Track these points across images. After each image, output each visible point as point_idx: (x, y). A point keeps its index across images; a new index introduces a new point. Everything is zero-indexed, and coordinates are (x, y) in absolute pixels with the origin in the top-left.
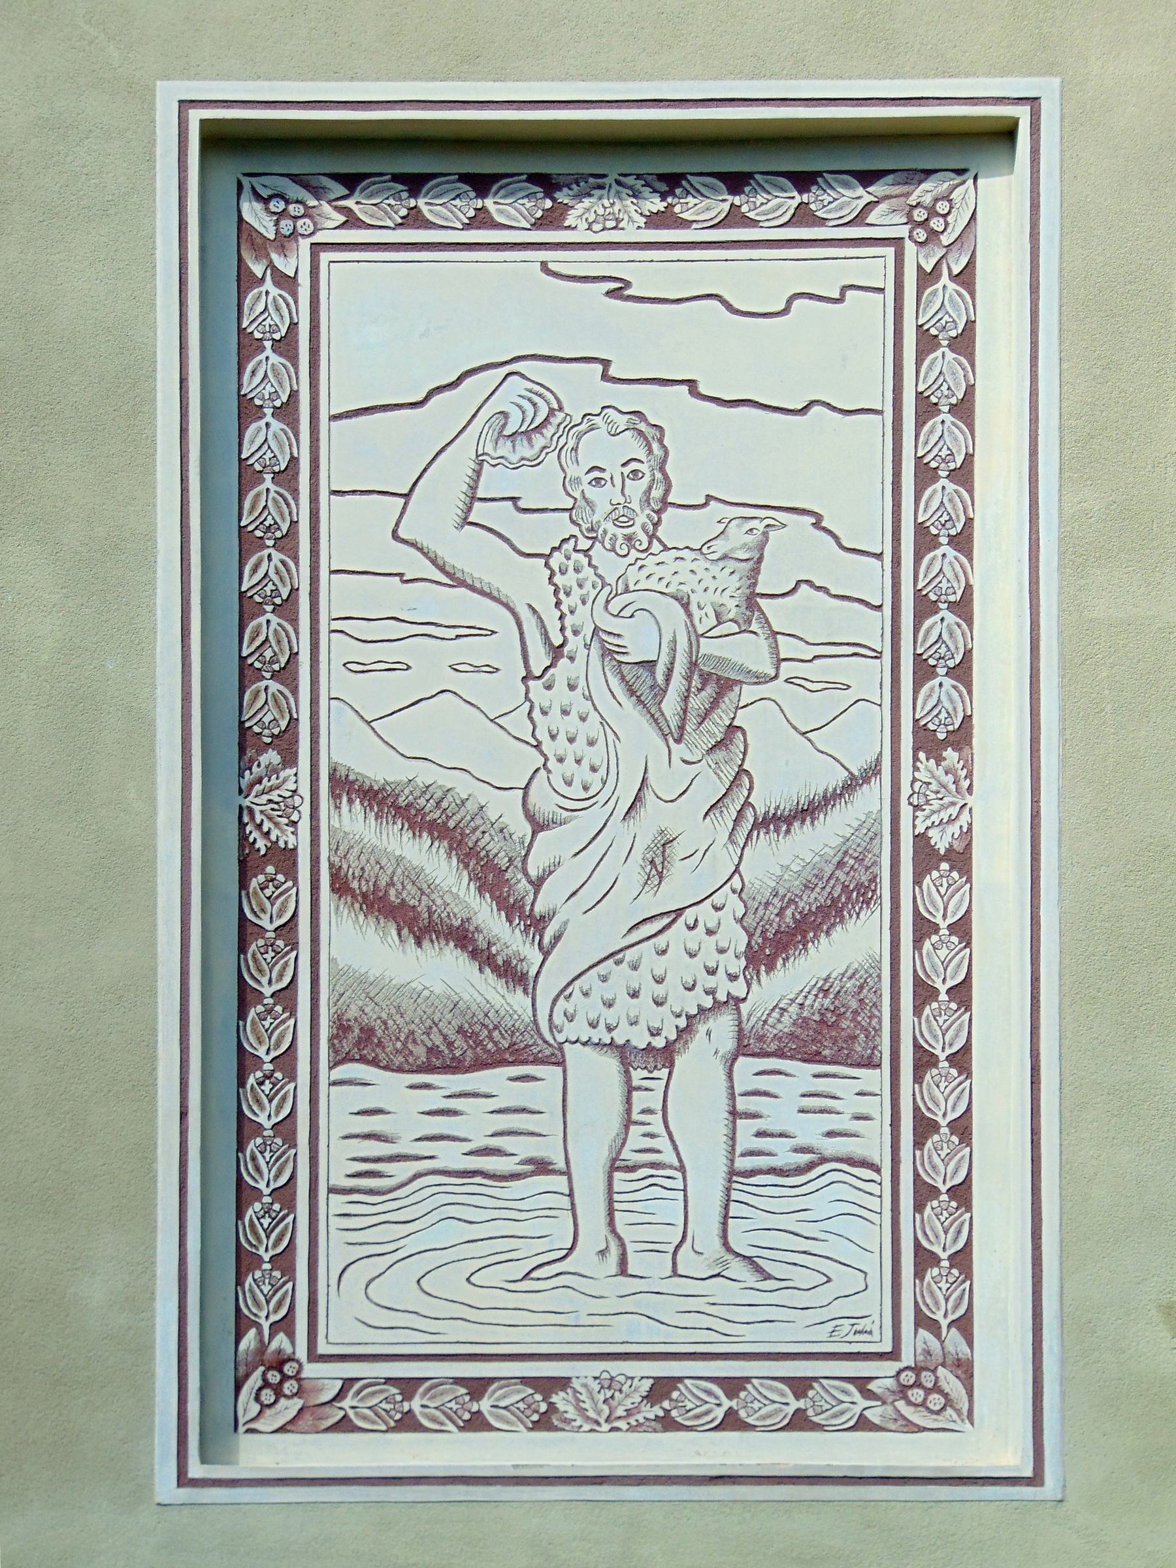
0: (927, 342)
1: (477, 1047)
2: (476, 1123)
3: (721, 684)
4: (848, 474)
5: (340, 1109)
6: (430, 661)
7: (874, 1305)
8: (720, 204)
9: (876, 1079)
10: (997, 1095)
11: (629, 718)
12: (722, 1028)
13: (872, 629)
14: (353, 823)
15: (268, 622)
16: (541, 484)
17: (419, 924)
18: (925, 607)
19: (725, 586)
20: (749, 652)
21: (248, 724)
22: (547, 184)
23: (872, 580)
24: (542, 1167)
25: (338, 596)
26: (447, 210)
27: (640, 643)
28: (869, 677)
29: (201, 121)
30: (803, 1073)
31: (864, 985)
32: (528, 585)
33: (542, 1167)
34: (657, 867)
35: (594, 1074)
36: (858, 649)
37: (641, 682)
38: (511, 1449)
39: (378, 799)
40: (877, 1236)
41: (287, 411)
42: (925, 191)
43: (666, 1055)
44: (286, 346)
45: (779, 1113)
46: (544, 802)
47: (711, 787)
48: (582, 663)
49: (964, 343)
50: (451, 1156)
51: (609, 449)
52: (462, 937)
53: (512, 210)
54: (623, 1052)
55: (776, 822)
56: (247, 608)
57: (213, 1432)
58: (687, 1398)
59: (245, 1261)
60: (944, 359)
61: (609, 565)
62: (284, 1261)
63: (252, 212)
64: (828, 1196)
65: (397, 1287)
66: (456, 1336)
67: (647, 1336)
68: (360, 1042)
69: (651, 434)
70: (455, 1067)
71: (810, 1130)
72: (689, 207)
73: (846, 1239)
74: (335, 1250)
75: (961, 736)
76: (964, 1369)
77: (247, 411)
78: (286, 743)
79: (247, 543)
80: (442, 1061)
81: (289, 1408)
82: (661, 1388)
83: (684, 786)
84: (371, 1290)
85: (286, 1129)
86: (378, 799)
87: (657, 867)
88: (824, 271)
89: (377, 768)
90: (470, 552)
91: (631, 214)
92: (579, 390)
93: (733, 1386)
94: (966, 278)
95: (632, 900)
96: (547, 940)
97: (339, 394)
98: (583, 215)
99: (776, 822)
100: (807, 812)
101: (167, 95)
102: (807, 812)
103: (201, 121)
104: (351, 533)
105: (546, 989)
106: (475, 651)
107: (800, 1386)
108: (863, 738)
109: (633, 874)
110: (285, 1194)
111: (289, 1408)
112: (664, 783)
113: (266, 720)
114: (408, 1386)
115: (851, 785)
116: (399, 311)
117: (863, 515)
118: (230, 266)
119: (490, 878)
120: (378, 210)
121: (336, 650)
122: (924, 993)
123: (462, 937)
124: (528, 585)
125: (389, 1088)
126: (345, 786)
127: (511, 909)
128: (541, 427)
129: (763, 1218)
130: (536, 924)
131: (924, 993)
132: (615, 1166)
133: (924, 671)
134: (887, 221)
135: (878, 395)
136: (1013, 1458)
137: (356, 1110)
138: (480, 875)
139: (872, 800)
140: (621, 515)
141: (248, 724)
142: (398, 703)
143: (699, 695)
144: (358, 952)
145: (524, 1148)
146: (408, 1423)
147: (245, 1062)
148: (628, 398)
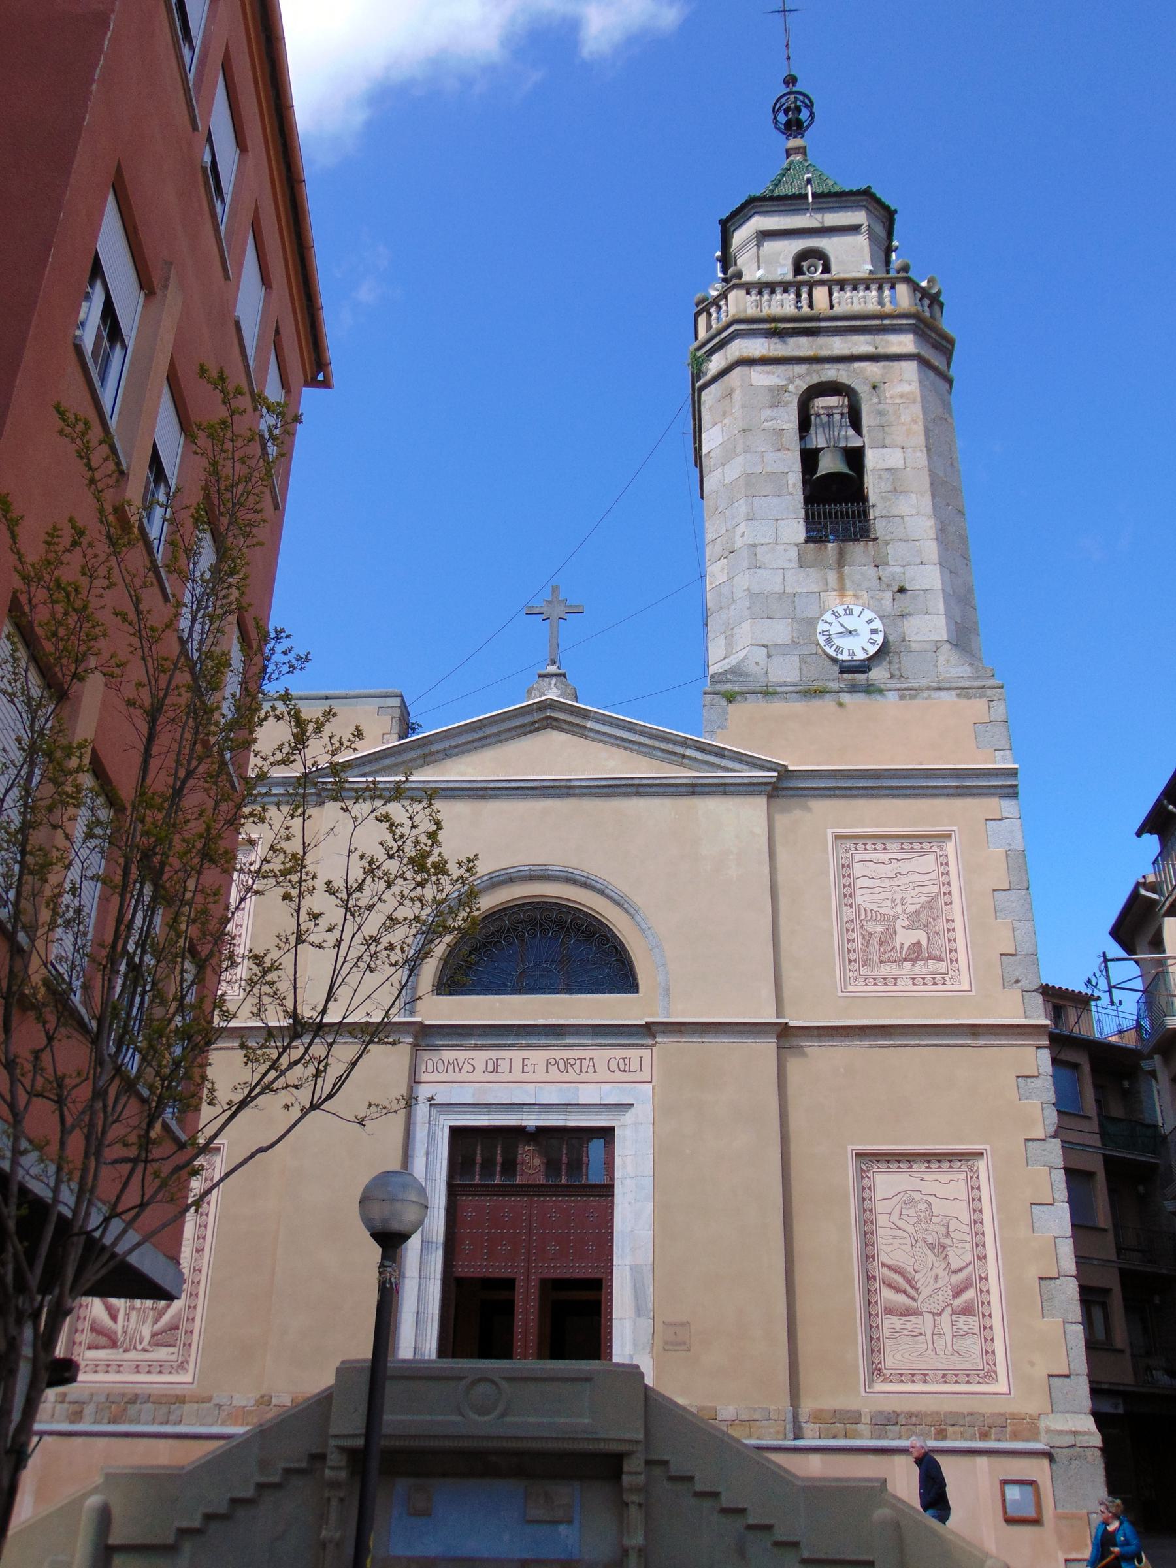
0: (972, 1188)
1: (907, 1312)
2: (909, 1326)
3: (944, 1247)
4: (962, 1211)
5: (886, 1323)
6: (896, 1242)
7: (979, 1361)
8: (938, 1165)
9: (976, 1319)
10: (996, 1321)
11: (929, 1253)
12: (949, 1309)
13: (968, 1238)
14: (885, 1271)
15: (869, 1236)
16: (912, 1212)
17: (898, 1290)
18: (976, 1234)
19: (943, 1230)
20: (948, 1241)
21: (868, 1257)
22: (909, 1161)
23: (967, 1229)
24: (921, 1334)
25: (881, 1231)
26: (894, 1165)
27: (930, 1240)
28: (968, 1246)
29: (637, 992)
30: (963, 1318)
31: (973, 1302)
32: (911, 1229)
33: (921, 1334)
34: (936, 1280)
35: (928, 1317)
36: (967, 1242)
37: (931, 1247)
38: (919, 1387)
39: (889, 1267)
40: (978, 1348)
41: (870, 1200)
42: (970, 1163)
43: (940, 1314)
44: (869, 1188)
45: (960, 1325)
46: (916, 1268)
47: (944, 1265)
48: (921, 1243)
49: (978, 1188)
50: (905, 1332)
51: (922, 1206)
52: (905, 1292)
53: (904, 1165)
54: (933, 1314)
55: (955, 1272)
56: (866, 1233)
57: (871, 1383)
58: (948, 1378)
59: (873, 1351)
60: (975, 1191)
61: (924, 1226)
62: (879, 1351)
63: (864, 1167)
64: (969, 1340)
65: (898, 1356)
66: (909, 1365)
67: (941, 1366)
68: (889, 1311)
69: (929, 1204)
70: (905, 1316)
71: (966, 1328)
72: (932, 1165)
73: (973, 1346)
74: (887, 1350)
75: (985, 1257)
76: (995, 1372)
77: (864, 1200)
78: (873, 1257)
79: (865, 1222)
80: (902, 1315)
81: (882, 1378)
82: (944, 1376)
83: (940, 1264)
84: (892, 1359)
85: (878, 1327)
86: (889, 1267)
87: (936, 1280)
88: (955, 1176)
89: (889, 1262)
90: (901, 1224)
91: (923, 1166)
92: (917, 1196)
93: (956, 1375)
94: (978, 1178)
95: (932, 1286)
96: (699, 384)
97: (879, 1196)
98: (915, 1167)
99: (955, 1272)
100: (960, 1270)
101: (850, 1148)
102: (960, 1270)
103: (637, 992)
104: (882, 1220)
105: (920, 1301)
106: (904, 1241)
107: (968, 1375)
108: (968, 1257)
109: (932, 1282)
110: (878, 1339)
111: (882, 1378)
112: (936, 1264)
113: (870, 1253)
114: (901, 1375)
115: (967, 1265)
116: (888, 1183)
117: (965, 1217)
118: (861, 1175)
119: (908, 1281)
120: (883, 1165)
121: (881, 1241)
122: (983, 1303)
123: (905, 1292)
124: (911, 1229)
125: (894, 1319)
126: (883, 1265)
127: (912, 1287)
128: (911, 1202)
129: (959, 1343)
130: (917, 1290)
131: (983, 1303)
132: (933, 1334)
133: (977, 1245)
134: (964, 1168)
135: (965, 1197)
136: (1005, 1390)
137: (890, 1323)
138: (906, 1282)
139: (971, 1268)
140: (925, 1217)
141: (868, 1257)
142: (891, 1251)
143: (940, 1249)
144: (887, 1294)
145: (918, 1331)
146: (902, 1381)
147: (870, 1315)
148: (925, 1197)
